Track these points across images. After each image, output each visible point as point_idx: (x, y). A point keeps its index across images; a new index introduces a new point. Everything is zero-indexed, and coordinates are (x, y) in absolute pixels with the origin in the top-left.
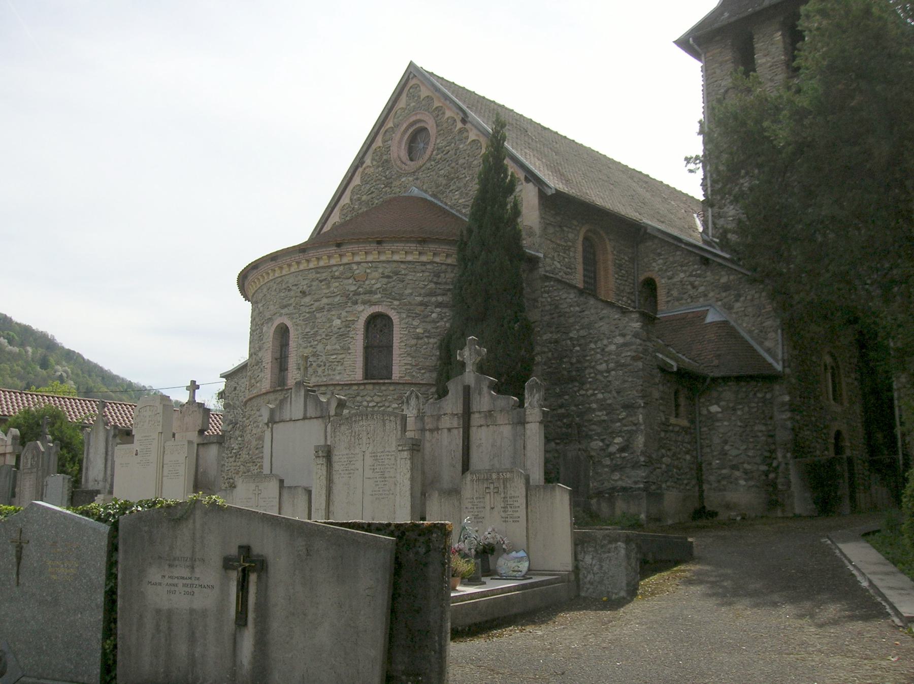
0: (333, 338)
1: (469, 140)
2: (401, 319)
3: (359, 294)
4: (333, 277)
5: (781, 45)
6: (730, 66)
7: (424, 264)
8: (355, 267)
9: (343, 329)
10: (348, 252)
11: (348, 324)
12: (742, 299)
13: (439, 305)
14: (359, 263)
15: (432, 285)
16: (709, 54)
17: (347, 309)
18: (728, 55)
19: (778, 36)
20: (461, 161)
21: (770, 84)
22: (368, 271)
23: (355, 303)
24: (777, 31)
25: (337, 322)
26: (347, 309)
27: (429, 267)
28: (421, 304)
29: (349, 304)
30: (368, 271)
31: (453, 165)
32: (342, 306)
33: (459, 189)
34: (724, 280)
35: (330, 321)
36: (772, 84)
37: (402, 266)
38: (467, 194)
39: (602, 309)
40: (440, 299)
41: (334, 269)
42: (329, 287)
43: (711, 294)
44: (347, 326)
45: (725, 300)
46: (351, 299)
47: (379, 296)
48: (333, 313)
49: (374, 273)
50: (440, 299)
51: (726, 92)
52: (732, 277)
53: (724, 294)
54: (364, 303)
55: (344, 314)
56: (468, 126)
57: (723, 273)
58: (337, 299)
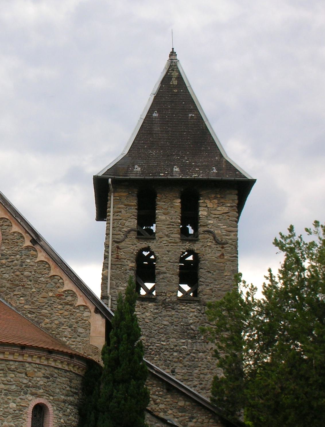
0: (9, 417)
1: (38, 260)
2: (54, 411)
3: (29, 387)
4: (9, 369)
5: (179, 210)
6: (134, 211)
7: (66, 371)
8: (27, 365)
9: (17, 412)
10: (27, 353)
11: (21, 408)
12: (194, 420)
13: (71, 403)
14: (30, 363)
15: (68, 388)
16: (116, 194)
17: (21, 397)
18: (134, 202)
19: (178, 202)
20: (26, 273)
21: (166, 238)
22: (36, 370)
23: (26, 393)
24: (177, 198)
25: (13, 405)
26: (21, 397)
27: (68, 374)
28: (64, 402)
29: (22, 393)
30: (36, 370)
31: (18, 273)
32: (17, 393)
33: (23, 296)
34: (181, 403)
35: (7, 403)
36: (168, 239)
37: (56, 371)
38: (33, 303)
39: (156, 423)
40: (71, 399)
41: (11, 363)
42: (6, 376)
43: (170, 412)
44: (20, 410)
45: (181, 419)
46: (24, 389)
47: (42, 391)
48: (10, 397)
49: (39, 373)
50: (71, 399)
51: (129, 232)
52: (187, 403)
53: (180, 414)
54: (32, 394)
55: (18, 400)
56: (37, 247)
57: (180, 398)
58: (14, 387)
